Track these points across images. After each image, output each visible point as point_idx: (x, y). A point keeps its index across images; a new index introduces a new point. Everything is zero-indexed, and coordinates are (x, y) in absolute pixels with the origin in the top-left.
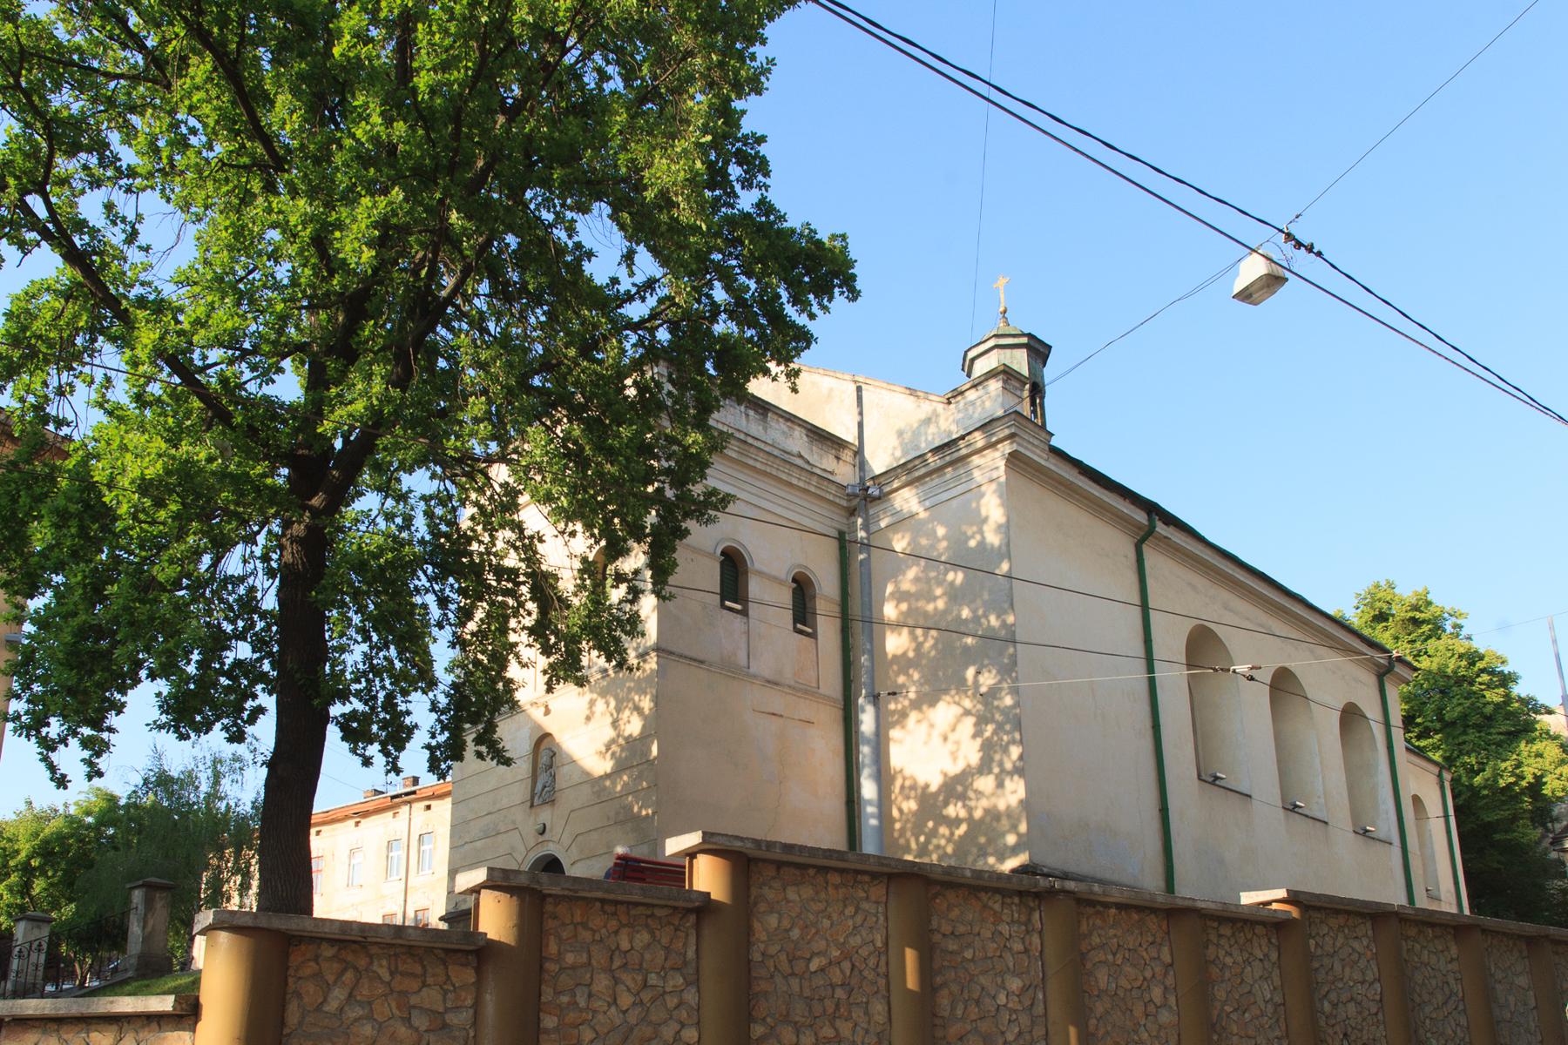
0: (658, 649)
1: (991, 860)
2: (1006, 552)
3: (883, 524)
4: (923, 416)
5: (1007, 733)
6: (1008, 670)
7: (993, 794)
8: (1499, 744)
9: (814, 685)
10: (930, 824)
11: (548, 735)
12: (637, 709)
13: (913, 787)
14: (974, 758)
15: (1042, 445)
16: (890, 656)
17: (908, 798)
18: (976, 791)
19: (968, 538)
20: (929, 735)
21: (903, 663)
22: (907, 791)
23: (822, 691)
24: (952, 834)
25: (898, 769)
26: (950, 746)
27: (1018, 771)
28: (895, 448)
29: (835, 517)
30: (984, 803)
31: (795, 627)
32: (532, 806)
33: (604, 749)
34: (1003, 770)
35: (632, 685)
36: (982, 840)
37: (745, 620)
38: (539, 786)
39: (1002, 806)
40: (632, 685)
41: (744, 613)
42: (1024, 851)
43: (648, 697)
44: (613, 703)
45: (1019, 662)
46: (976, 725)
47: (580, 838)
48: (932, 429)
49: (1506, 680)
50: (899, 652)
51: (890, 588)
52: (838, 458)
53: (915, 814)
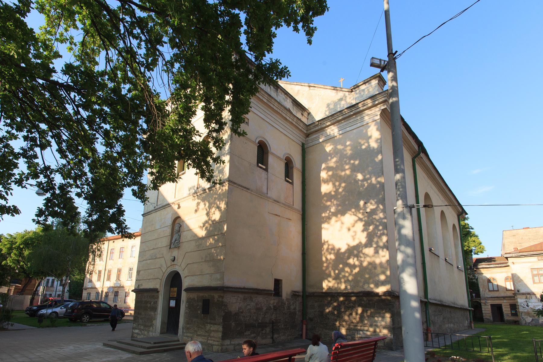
0: (229, 180)
1: (372, 286)
3: (321, 140)
4: (339, 98)
7: (373, 256)
9: (292, 204)
10: (341, 266)
11: (179, 217)
12: (218, 208)
13: (333, 249)
14: (364, 241)
16: (323, 193)
17: (330, 253)
18: (364, 254)
19: (361, 145)
20: (341, 227)
21: (329, 196)
23: (295, 206)
24: (352, 271)
25: (326, 240)
26: (351, 233)
28: (326, 111)
29: (301, 137)
30: (368, 259)
31: (285, 179)
32: (170, 248)
33: (202, 225)
35: (217, 196)
36: (367, 276)
38: (174, 240)
39: (378, 261)
40: (217, 196)
41: (266, 170)
42: (388, 284)
43: (224, 202)
44: (207, 204)
45: (386, 199)
46: (364, 225)
47: (188, 265)
48: (343, 102)
50: (328, 192)
51: (324, 166)
52: (302, 115)
53: (334, 260)
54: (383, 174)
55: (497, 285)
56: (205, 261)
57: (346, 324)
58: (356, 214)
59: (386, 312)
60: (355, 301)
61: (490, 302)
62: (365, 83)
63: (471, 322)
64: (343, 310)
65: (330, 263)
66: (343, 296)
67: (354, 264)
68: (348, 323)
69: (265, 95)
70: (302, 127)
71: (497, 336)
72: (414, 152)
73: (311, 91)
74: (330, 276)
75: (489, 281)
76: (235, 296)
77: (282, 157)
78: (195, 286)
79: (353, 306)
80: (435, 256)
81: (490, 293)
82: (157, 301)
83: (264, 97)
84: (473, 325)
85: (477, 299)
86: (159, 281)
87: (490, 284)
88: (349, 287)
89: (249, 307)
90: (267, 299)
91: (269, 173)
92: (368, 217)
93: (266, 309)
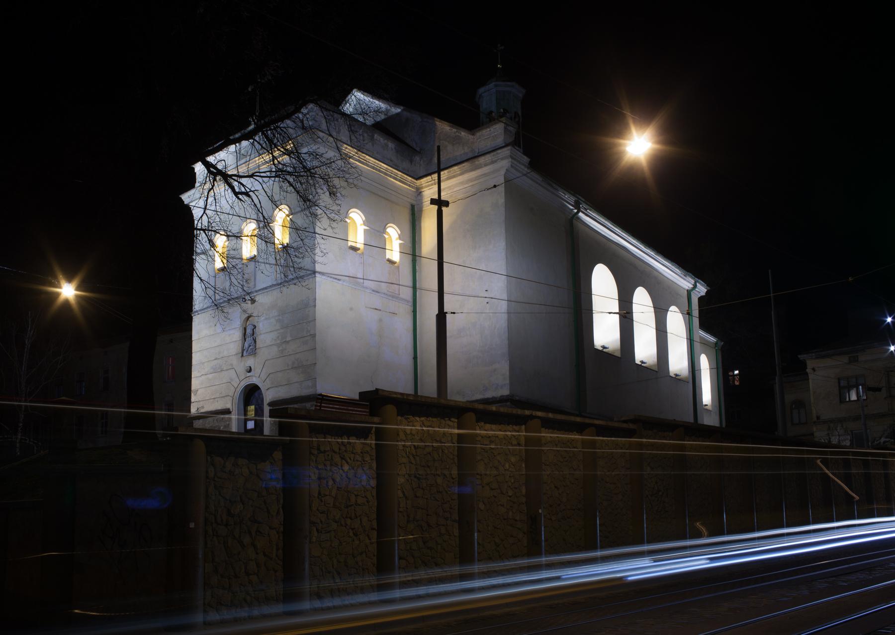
23: (401, 296)
32: (242, 356)
44: (256, 232)
47: (271, 376)
56: (292, 368)
78: (281, 399)
82: (229, 424)
86: (230, 399)
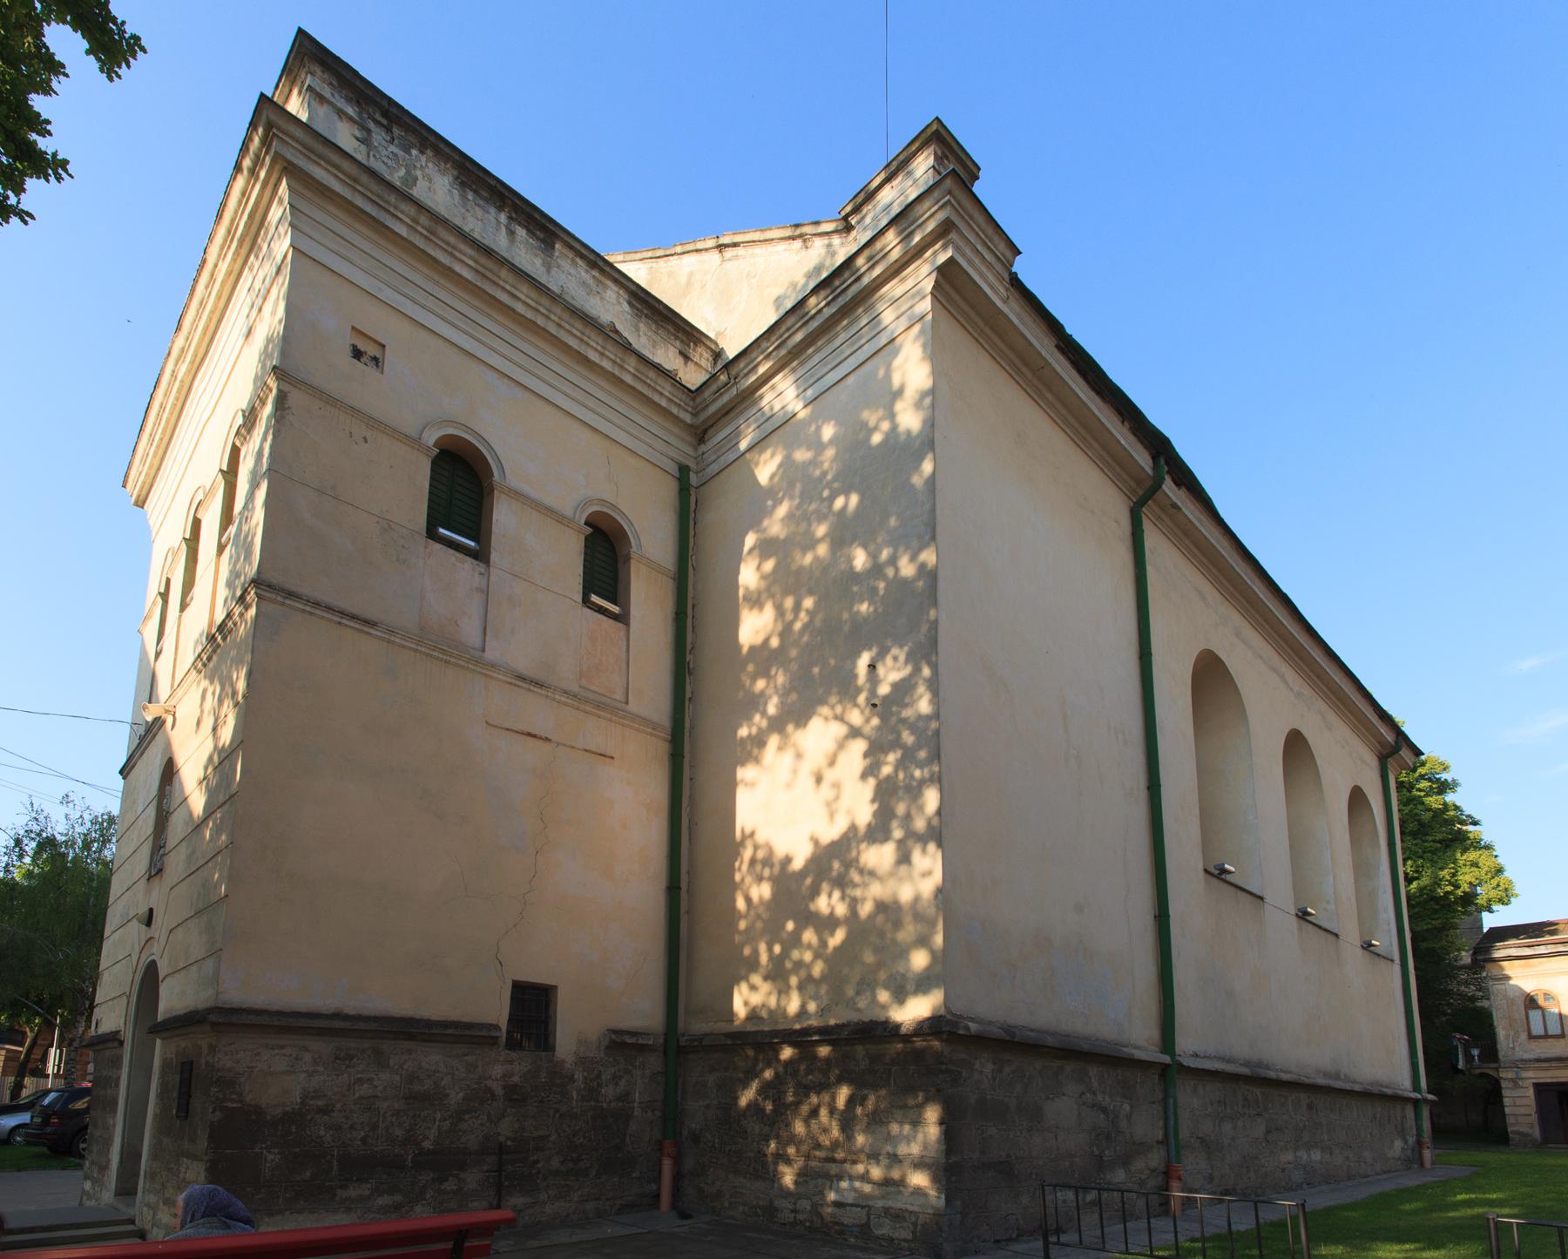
1: (884, 996)
2: (927, 442)
3: (743, 445)
5: (920, 765)
6: (926, 651)
7: (892, 874)
8: (1433, 852)
9: (619, 696)
10: (790, 926)
13: (768, 862)
14: (864, 814)
15: (998, 267)
16: (745, 650)
17: (760, 879)
20: (795, 772)
21: (764, 657)
22: (758, 867)
23: (633, 707)
25: (748, 831)
26: (826, 791)
27: (936, 835)
29: (672, 440)
30: (876, 890)
34: (911, 835)
37: (482, 568)
39: (906, 894)
41: (481, 555)
49: (1444, 787)
50: (759, 640)
51: (750, 540)
52: (687, 358)
54: (933, 538)
55: (1560, 1015)
57: (798, 1151)
58: (844, 712)
59: (927, 1100)
60: (827, 1060)
61: (1532, 1076)
62: (888, 180)
63: (1420, 1142)
64: (790, 1098)
65: (758, 917)
66: (793, 1044)
67: (832, 913)
68: (804, 1148)
69: (462, 247)
70: (670, 400)
71: (1488, 1196)
72: (1139, 483)
73: (728, 265)
74: (753, 965)
75: (1531, 1002)
76: (282, 1047)
77: (568, 512)
79: (821, 1084)
80: (1239, 892)
81: (1534, 1044)
83: (457, 258)
84: (1427, 1154)
85: (1486, 1065)
87: (1535, 1016)
88: (812, 1007)
89: (364, 1090)
90: (470, 1058)
91: (491, 569)
92: (884, 718)
93: (464, 1099)
